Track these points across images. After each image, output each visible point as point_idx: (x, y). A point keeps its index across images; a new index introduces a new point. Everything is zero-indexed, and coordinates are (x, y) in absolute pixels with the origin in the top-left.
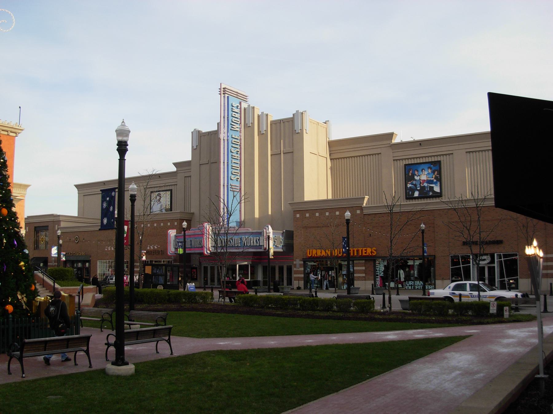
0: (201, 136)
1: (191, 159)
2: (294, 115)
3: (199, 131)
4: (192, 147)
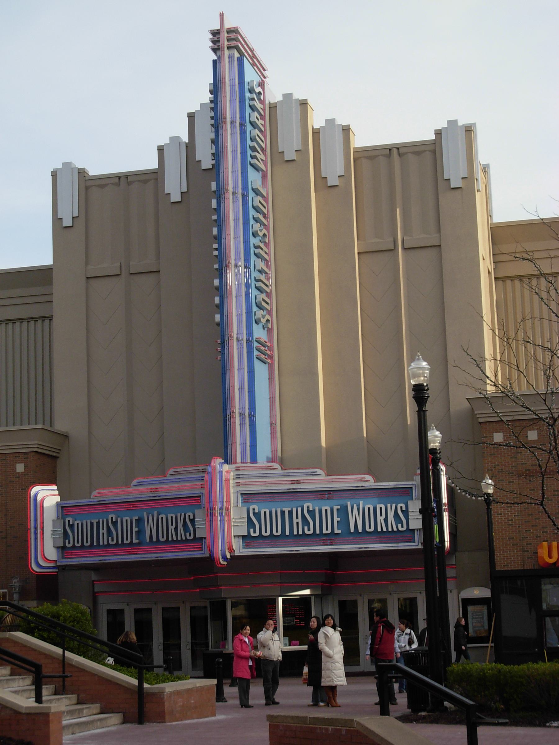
0: (87, 188)
1: (51, 263)
2: (438, 133)
3: (82, 172)
4: (57, 220)
